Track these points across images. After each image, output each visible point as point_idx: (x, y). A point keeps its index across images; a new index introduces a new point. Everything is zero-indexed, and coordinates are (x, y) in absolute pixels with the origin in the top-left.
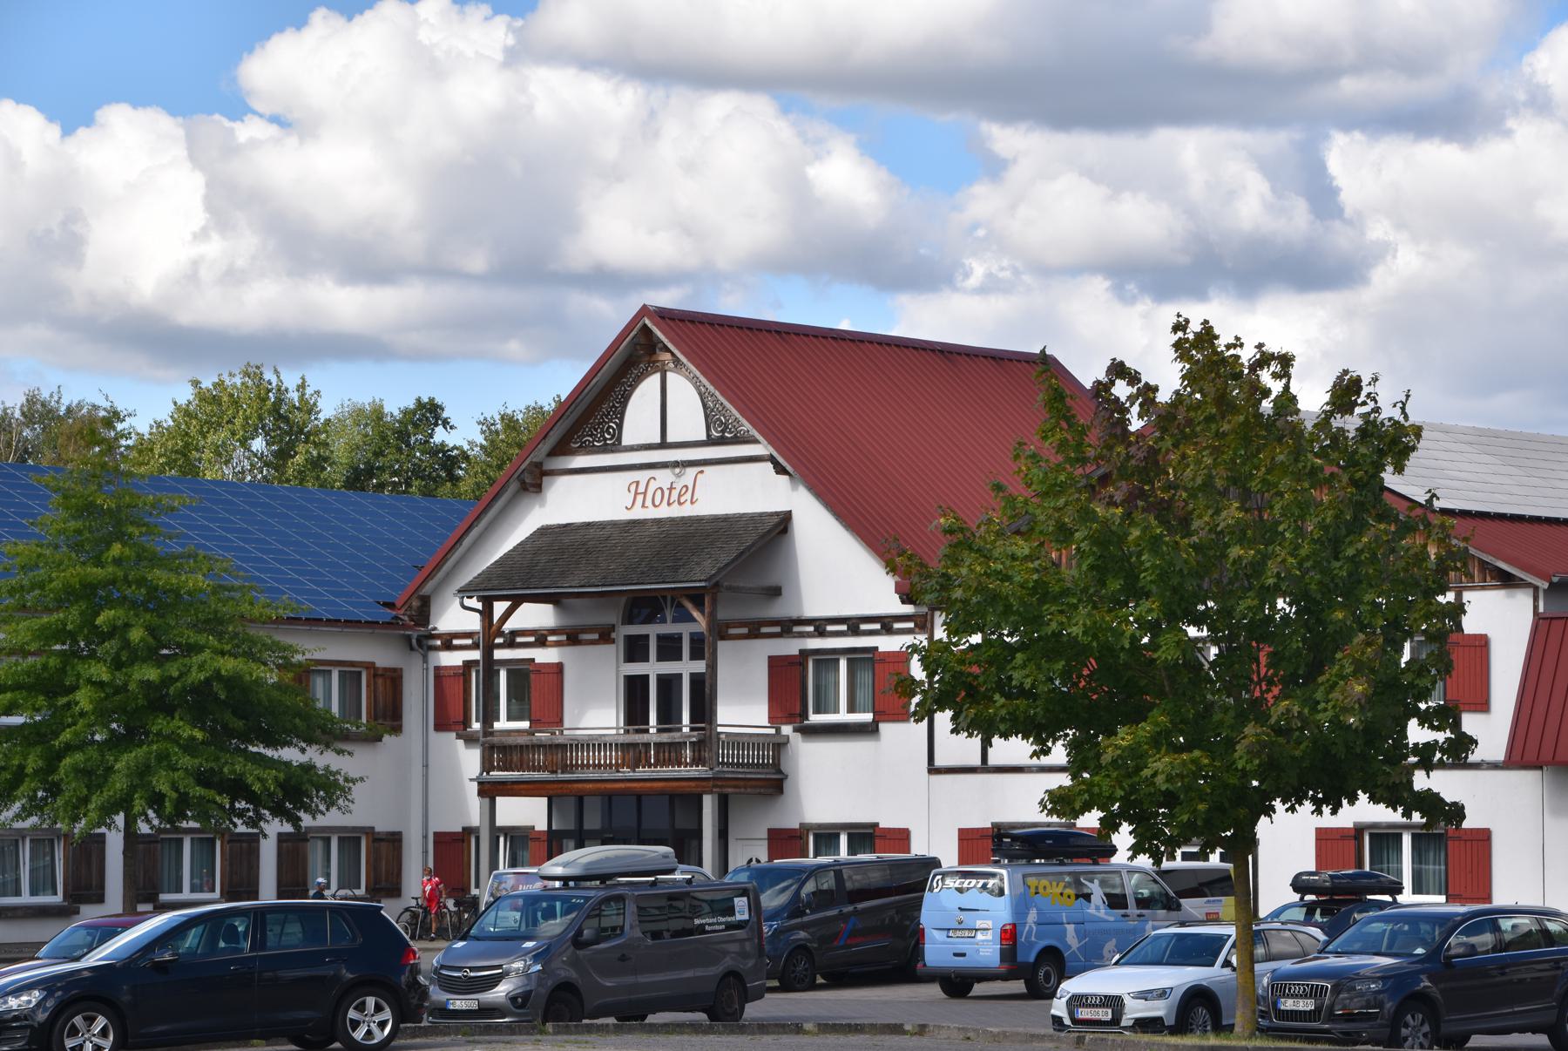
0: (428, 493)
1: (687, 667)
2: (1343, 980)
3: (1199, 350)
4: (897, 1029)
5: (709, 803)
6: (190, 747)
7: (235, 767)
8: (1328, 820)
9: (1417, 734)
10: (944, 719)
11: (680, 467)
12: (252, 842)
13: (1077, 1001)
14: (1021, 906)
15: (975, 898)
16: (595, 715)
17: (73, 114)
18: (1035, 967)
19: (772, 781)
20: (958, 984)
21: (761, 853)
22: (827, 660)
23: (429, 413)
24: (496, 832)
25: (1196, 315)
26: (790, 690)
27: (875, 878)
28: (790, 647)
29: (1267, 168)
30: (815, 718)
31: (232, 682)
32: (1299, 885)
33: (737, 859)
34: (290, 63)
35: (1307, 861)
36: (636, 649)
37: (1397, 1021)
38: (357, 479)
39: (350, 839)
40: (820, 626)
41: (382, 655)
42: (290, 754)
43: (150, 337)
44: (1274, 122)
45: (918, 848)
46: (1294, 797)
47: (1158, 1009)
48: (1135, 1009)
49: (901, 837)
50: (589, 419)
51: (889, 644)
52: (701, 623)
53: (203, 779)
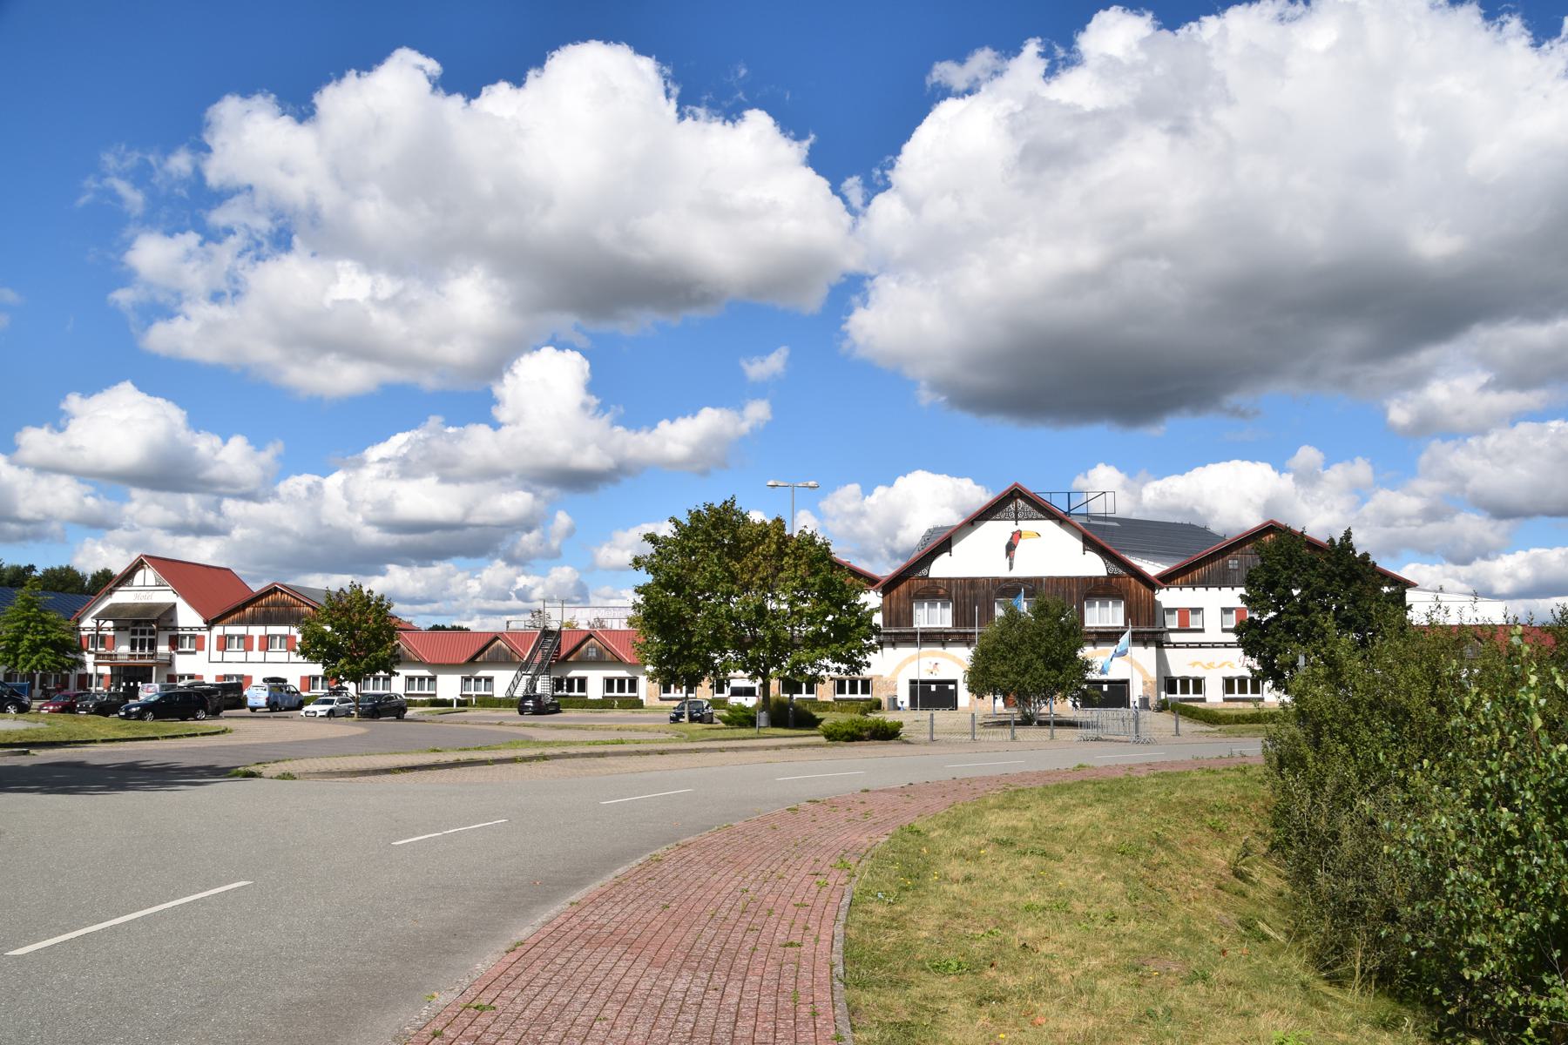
11: (147, 591)
19: (170, 663)
22: (184, 637)
23: (32, 568)
31: (63, 640)
36: (134, 632)
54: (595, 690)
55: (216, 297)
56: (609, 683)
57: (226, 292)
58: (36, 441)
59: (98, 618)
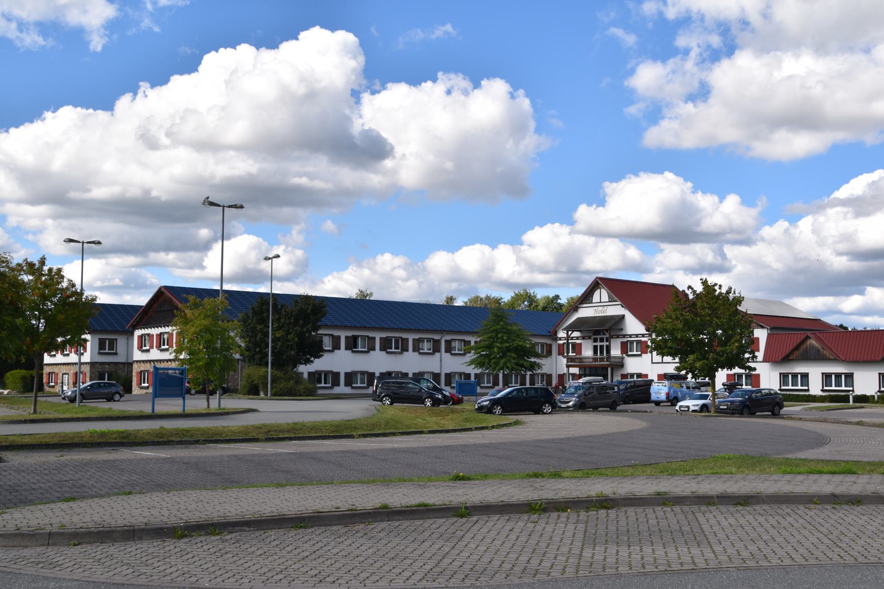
0: (557, 312)
1: (605, 344)
2: (732, 402)
3: (704, 283)
4: (646, 412)
5: (609, 369)
6: (514, 358)
7: (522, 362)
8: (730, 372)
9: (747, 355)
10: (655, 353)
11: (604, 306)
12: (525, 376)
13: (681, 407)
14: (670, 389)
15: (661, 387)
16: (587, 352)
17: (494, 246)
18: (673, 400)
19: (621, 365)
20: (658, 403)
21: (619, 378)
23: (557, 297)
24: (569, 374)
25: (704, 277)
26: (625, 348)
27: (642, 383)
28: (625, 340)
29: (713, 251)
30: (163, 347)
31: (522, 346)
32: (723, 385)
33: (615, 380)
34: (531, 236)
35: (725, 380)
36: (595, 340)
37: (742, 410)
38: (544, 309)
39: (543, 375)
40: (630, 336)
41: (548, 341)
42: (533, 360)
43: (507, 285)
44: (713, 242)
45: (650, 378)
46: (723, 368)
47: (696, 408)
48: (692, 408)
49: (646, 376)
50: (586, 298)
51: (643, 339)
52: (608, 336)
53: (516, 364)
54: (815, 387)
55: (691, 98)
56: (827, 377)
57: (701, 93)
58: (584, 214)
59: (567, 329)
